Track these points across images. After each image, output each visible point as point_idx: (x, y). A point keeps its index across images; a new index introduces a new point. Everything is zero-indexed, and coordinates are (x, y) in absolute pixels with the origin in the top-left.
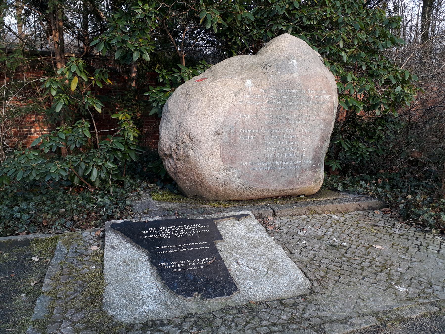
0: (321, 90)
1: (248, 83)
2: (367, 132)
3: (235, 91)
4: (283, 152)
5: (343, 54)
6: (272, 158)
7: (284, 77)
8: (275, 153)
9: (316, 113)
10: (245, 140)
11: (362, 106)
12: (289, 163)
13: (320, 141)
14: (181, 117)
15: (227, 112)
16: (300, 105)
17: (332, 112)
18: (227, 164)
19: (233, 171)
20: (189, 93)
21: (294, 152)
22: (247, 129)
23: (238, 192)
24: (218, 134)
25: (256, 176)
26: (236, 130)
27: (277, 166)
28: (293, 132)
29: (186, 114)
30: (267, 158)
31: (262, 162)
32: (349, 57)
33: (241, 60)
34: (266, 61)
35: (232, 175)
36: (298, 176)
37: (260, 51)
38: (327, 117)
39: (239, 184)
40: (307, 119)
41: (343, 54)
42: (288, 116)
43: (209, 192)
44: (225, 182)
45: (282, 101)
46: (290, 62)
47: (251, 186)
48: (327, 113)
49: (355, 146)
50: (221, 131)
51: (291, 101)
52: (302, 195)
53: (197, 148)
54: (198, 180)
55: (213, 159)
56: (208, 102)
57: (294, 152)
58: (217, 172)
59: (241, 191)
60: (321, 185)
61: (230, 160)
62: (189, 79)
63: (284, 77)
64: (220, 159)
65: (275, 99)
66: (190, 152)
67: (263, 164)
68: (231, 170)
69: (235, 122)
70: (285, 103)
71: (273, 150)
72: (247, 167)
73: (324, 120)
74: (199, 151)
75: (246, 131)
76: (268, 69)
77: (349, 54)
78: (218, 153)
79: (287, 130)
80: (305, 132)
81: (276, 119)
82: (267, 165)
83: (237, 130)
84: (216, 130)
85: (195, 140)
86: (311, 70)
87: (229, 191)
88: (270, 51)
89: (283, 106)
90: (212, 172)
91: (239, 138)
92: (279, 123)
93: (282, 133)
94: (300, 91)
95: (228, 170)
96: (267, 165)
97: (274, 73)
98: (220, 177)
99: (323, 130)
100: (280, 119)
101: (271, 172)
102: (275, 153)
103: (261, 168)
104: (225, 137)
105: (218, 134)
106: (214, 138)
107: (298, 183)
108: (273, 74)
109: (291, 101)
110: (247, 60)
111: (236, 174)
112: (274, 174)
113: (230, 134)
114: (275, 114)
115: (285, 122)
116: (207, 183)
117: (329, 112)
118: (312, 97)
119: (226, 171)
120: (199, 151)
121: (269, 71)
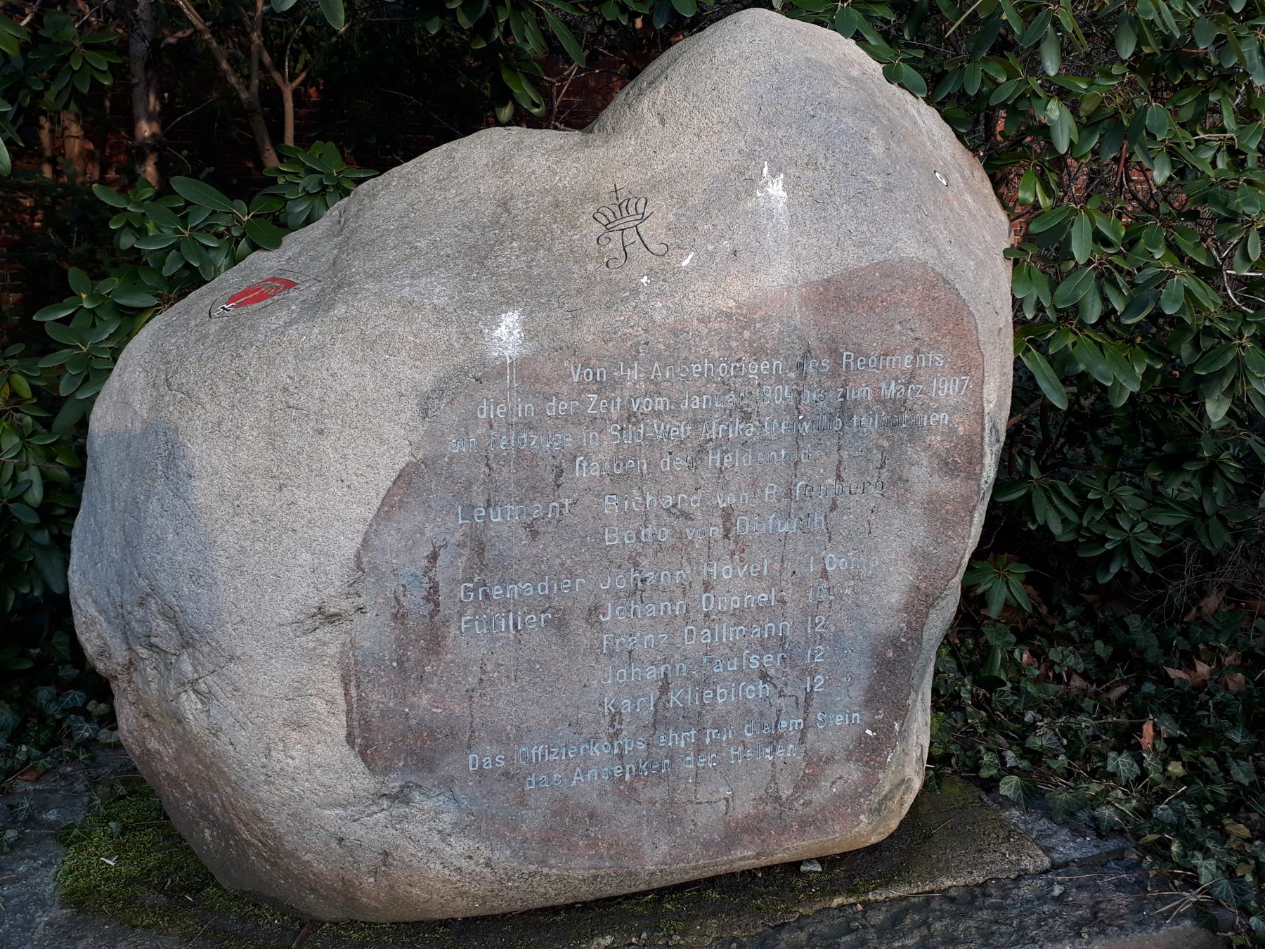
0: (917, 352)
1: (501, 331)
2: (1156, 432)
3: (427, 380)
4: (707, 682)
5: (1054, 112)
6: (647, 717)
7: (712, 293)
8: (665, 688)
9: (885, 474)
10: (494, 640)
11: (1139, 370)
12: (739, 733)
13: (906, 609)
14: (134, 507)
15: (377, 503)
16: (799, 436)
17: (973, 449)
18: (387, 770)
19: (428, 805)
20: (175, 382)
21: (764, 677)
22: (502, 583)
23: (462, 894)
24: (332, 619)
25: (555, 813)
26: (434, 588)
27: (672, 754)
28: (760, 578)
29: (154, 505)
30: (615, 717)
31: (593, 739)
32: (1087, 126)
33: (503, 165)
34: (629, 178)
35: (423, 823)
36: (786, 793)
37: (608, 116)
38: (948, 487)
39: (463, 863)
40: (834, 507)
41: (1054, 112)
42: (731, 499)
43: (313, 890)
44: (386, 854)
45: (695, 423)
46: (750, 194)
47: (532, 868)
48: (947, 467)
49: (1098, 504)
50: (345, 605)
51: (747, 417)
52: (809, 861)
53: (216, 689)
54: (246, 835)
55: (310, 750)
56: (271, 444)
57: (764, 677)
58: (340, 811)
59: (473, 889)
60: (907, 807)
61: (400, 748)
62: (235, 260)
63: (712, 293)
64: (346, 749)
65: (658, 414)
66: (189, 704)
67: (595, 751)
68: (417, 796)
69: (426, 551)
70: (716, 430)
71: (652, 674)
72: (506, 774)
73: (932, 507)
74: (233, 705)
75: (496, 592)
76: (631, 236)
77: (1086, 108)
78: (332, 720)
79: (724, 570)
80: (824, 573)
81: (667, 519)
82: (621, 756)
83: (443, 589)
84: (315, 601)
85: (206, 649)
86: (862, 245)
87: (415, 891)
88: (651, 119)
89: (702, 450)
90: (308, 810)
91: (453, 631)
92: (681, 536)
93: (698, 587)
94: (800, 366)
95: (401, 797)
96: (621, 756)
97: (655, 262)
98: (356, 831)
99: (925, 556)
100: (687, 516)
101: (639, 785)
102: (665, 688)
103: (585, 772)
104: (372, 631)
105: (332, 619)
106: (309, 641)
107: (785, 829)
108: (651, 272)
109: (747, 417)
110: (534, 166)
111: (446, 817)
112: (660, 793)
113: (399, 617)
114: (659, 495)
115: (717, 532)
116: (292, 855)
117: (958, 462)
118: (862, 392)
119: (385, 803)
120: (233, 705)
121: (636, 251)
